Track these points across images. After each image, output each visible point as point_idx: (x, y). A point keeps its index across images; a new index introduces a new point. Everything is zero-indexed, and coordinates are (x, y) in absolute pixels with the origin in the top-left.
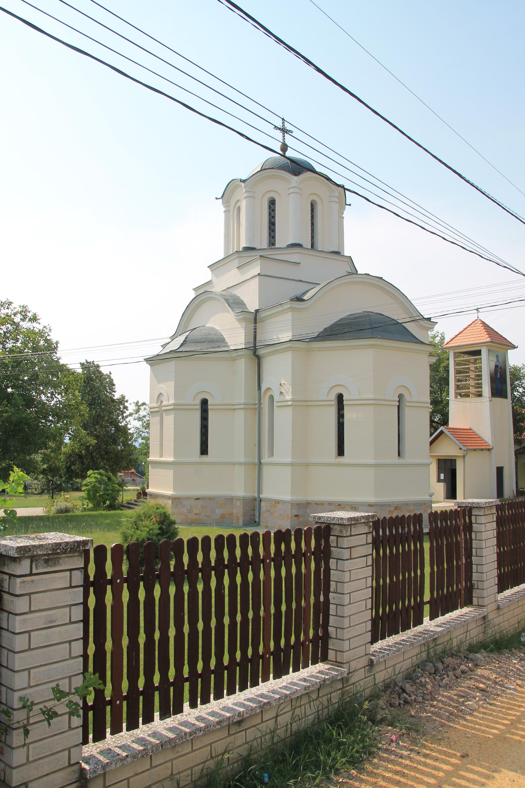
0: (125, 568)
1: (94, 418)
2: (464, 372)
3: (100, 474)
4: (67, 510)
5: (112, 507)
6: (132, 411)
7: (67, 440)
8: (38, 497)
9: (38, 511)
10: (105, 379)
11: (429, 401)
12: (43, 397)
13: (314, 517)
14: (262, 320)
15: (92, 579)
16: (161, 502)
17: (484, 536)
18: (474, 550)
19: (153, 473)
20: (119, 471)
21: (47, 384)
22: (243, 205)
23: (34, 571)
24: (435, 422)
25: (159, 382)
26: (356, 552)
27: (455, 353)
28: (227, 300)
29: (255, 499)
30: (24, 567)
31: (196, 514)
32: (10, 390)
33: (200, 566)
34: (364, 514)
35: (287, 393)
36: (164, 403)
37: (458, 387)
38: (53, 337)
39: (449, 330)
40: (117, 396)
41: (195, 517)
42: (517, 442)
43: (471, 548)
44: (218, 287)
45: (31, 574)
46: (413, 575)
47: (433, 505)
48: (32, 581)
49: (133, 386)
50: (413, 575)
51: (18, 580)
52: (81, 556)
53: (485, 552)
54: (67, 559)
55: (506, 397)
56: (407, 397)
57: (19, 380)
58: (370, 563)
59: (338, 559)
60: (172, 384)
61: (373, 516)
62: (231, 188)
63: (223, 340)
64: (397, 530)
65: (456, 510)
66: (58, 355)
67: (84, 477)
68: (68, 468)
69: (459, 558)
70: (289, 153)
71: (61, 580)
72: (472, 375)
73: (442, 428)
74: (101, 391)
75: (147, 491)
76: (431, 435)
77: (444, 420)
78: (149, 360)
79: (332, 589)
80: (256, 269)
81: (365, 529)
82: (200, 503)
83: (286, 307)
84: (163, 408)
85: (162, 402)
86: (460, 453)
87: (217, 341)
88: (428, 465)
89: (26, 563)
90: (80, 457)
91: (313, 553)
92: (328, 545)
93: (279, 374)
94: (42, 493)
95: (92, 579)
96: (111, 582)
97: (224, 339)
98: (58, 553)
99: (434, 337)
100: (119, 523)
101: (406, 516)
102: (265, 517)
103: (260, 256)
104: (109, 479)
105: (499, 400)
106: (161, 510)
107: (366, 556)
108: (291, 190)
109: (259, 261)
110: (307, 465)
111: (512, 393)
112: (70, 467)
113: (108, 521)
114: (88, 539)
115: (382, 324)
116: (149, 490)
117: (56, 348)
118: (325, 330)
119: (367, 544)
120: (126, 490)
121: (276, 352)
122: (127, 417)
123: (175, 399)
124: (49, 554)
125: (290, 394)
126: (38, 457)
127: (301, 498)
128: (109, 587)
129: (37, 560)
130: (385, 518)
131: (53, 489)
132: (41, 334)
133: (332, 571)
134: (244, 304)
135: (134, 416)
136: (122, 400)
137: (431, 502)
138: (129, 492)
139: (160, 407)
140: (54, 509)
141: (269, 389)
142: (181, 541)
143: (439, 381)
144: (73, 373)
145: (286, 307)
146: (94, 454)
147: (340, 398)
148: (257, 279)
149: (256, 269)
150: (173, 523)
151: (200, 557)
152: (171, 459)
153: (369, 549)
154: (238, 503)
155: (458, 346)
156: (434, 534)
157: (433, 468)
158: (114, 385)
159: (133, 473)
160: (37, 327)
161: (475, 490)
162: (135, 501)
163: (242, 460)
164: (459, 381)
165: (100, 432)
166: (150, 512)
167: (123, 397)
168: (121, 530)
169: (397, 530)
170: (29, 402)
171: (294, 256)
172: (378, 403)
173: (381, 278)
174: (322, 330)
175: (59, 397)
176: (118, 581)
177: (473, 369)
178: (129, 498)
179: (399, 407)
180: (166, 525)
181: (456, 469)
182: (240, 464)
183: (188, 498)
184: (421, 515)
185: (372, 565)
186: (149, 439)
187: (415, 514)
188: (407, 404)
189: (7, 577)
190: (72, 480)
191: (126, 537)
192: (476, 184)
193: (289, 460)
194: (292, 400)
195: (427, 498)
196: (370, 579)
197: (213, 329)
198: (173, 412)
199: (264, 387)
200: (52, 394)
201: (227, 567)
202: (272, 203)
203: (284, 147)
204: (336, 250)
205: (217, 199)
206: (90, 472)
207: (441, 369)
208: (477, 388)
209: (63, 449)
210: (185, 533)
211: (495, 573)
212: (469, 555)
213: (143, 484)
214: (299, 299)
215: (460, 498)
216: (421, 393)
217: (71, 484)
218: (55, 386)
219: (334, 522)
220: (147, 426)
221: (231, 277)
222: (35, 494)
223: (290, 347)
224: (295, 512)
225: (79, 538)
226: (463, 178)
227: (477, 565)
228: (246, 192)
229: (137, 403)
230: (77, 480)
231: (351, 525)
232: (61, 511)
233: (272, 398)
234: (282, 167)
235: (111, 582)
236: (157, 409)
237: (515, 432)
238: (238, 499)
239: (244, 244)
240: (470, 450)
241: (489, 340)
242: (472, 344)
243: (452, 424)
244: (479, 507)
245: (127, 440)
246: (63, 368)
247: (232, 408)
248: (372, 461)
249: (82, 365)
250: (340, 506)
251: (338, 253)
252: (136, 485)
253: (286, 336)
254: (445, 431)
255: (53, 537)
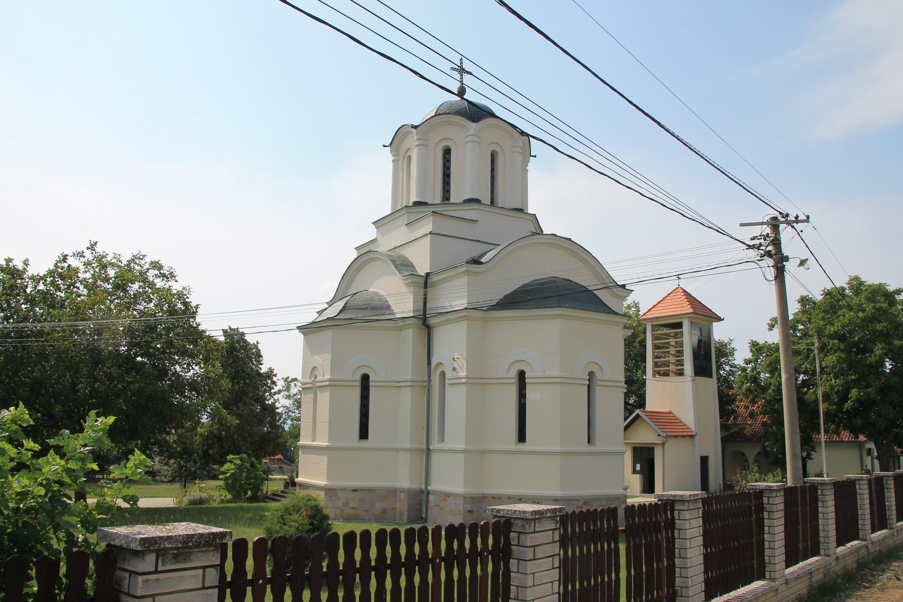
0: (268, 569)
1: (237, 393)
2: (663, 348)
3: (241, 460)
4: (201, 501)
5: (254, 499)
6: (281, 388)
7: (205, 419)
8: (167, 486)
9: (167, 502)
10: (251, 349)
11: (624, 380)
12: (178, 368)
13: (492, 510)
14: (434, 285)
15: (229, 579)
16: (311, 492)
17: (689, 533)
18: (677, 551)
19: (304, 459)
20: (264, 457)
21: (184, 353)
22: (414, 153)
23: (160, 568)
24: (630, 405)
25: (314, 353)
26: (541, 552)
27: (653, 326)
28: (393, 262)
29: (422, 492)
30: (148, 562)
31: (353, 508)
32: (139, 359)
33: (358, 566)
34: (550, 507)
35: (461, 369)
36: (319, 379)
37: (656, 365)
38: (193, 300)
39: (646, 299)
40: (264, 369)
41: (352, 512)
42: (724, 427)
43: (674, 548)
44: (384, 247)
45: (156, 572)
46: (606, 579)
47: (628, 500)
48: (158, 580)
49: (283, 358)
50: (606, 579)
51: (141, 578)
52: (217, 551)
53: (690, 553)
54: (200, 554)
55: (711, 376)
56: (598, 375)
57: (151, 347)
58: (557, 564)
59: (519, 560)
60: (328, 356)
61: (561, 510)
62: (401, 134)
63: (388, 307)
64: (588, 526)
65: (656, 504)
66: (198, 320)
67: (222, 464)
68: (205, 452)
69: (659, 561)
70: (469, 96)
71: (192, 579)
72: (672, 350)
73: (638, 411)
74: (245, 363)
75: (296, 480)
76: (626, 419)
77: (640, 402)
78: (303, 329)
79: (512, 596)
80: (427, 227)
81: (551, 525)
82: (357, 495)
83: (461, 270)
84: (318, 384)
85: (316, 377)
86: (658, 440)
87: (381, 308)
88: (623, 453)
89: (151, 558)
90: (220, 439)
91: (490, 552)
92: (508, 544)
93: (453, 347)
94: (172, 481)
95: (229, 579)
96: (251, 583)
97: (390, 306)
98: (190, 547)
99: (629, 307)
100: (262, 518)
101: (599, 510)
102: (433, 511)
103: (433, 212)
104: (252, 465)
105: (702, 380)
106: (312, 503)
107: (552, 556)
108: (469, 139)
109: (431, 218)
110: (483, 452)
111: (718, 372)
112: (207, 451)
113: (249, 515)
114: (225, 530)
115: (569, 291)
116: (300, 479)
117: (195, 313)
118: (506, 297)
119: (554, 542)
120: (271, 480)
121: (449, 322)
122: (275, 393)
123: (332, 373)
124: (179, 548)
125: (465, 371)
126: (171, 438)
127: (476, 491)
128: (249, 589)
129: (164, 555)
130: (574, 512)
131: (185, 477)
132: (181, 295)
133: (512, 574)
134: (413, 266)
135: (283, 393)
136: (270, 374)
137: (626, 497)
138: (275, 482)
139: (314, 382)
140: (186, 500)
141: (440, 364)
142: (336, 535)
143: (634, 357)
144: (214, 341)
145: (461, 270)
146: (236, 437)
147: (522, 375)
148: (428, 238)
149: (427, 227)
150: (326, 517)
151: (358, 554)
152: (325, 444)
153: (556, 549)
154: (402, 496)
155: (657, 318)
156: (632, 532)
157: (628, 457)
158: (261, 356)
159: (280, 459)
160: (176, 287)
161: (676, 480)
162: (282, 492)
163: (408, 445)
164: (657, 357)
165: (243, 411)
166: (300, 505)
167: (271, 370)
168: (265, 525)
169: (588, 526)
170: (163, 373)
171: (471, 213)
172: (565, 382)
173: (570, 239)
174: (501, 297)
175: (197, 368)
176: (261, 581)
177: (673, 344)
178: (275, 488)
179: (589, 386)
180: (317, 517)
181: (653, 459)
182: (405, 450)
183: (344, 490)
184: (616, 509)
185: (559, 567)
186: (299, 419)
187: (609, 508)
188: (599, 383)
189: (127, 575)
190: (207, 465)
191: (268, 530)
192: (676, 133)
193: (461, 446)
194: (467, 377)
195: (621, 491)
196: (556, 584)
197: (377, 294)
198: (328, 388)
199: (434, 362)
200: (189, 365)
201: (389, 567)
202: (447, 152)
203: (461, 92)
204: (519, 207)
205: (384, 146)
206: (230, 457)
207: (636, 344)
208: (677, 365)
209: (199, 430)
210: (340, 528)
211: (701, 577)
212: (671, 557)
213: (292, 472)
214: (476, 261)
215: (658, 489)
216: (614, 370)
217: (208, 471)
218: (193, 356)
219: (515, 516)
220: (298, 404)
221: (400, 235)
222: (164, 482)
223: (465, 316)
224: (469, 507)
225: (215, 530)
226: (662, 127)
227: (681, 568)
228: (418, 139)
229: (286, 380)
230: (215, 467)
231: (535, 520)
232: (193, 502)
233: (443, 374)
234: (460, 113)
235: (251, 583)
236: (310, 385)
237: (721, 417)
238: (402, 491)
239: (414, 198)
240: (670, 436)
241: (691, 310)
242: (672, 316)
243: (648, 407)
244: (682, 501)
245: (274, 420)
246: (200, 334)
247: (397, 386)
248: (558, 449)
249: (225, 332)
250: (520, 500)
251: (521, 210)
252: (284, 474)
253: (461, 303)
254: (642, 414)
255: (183, 528)
